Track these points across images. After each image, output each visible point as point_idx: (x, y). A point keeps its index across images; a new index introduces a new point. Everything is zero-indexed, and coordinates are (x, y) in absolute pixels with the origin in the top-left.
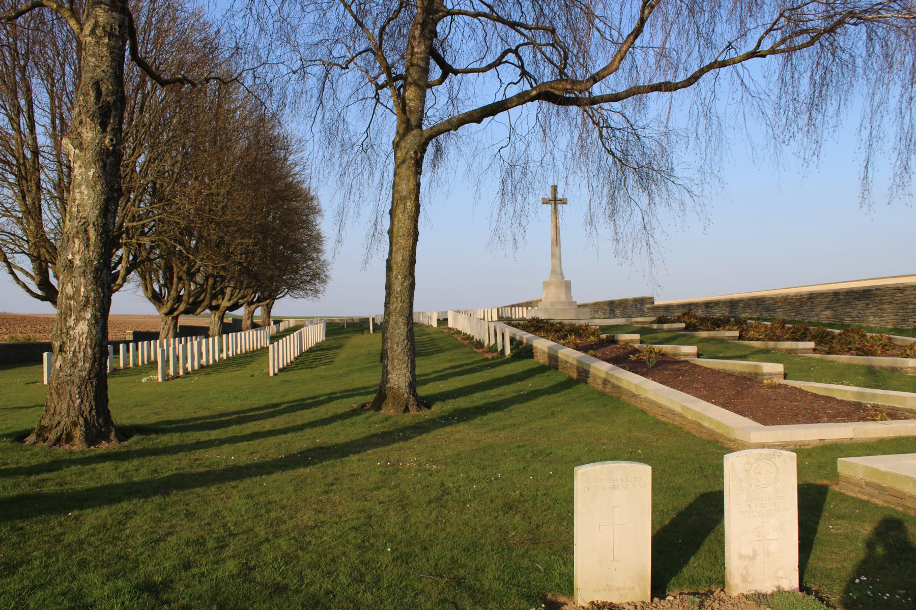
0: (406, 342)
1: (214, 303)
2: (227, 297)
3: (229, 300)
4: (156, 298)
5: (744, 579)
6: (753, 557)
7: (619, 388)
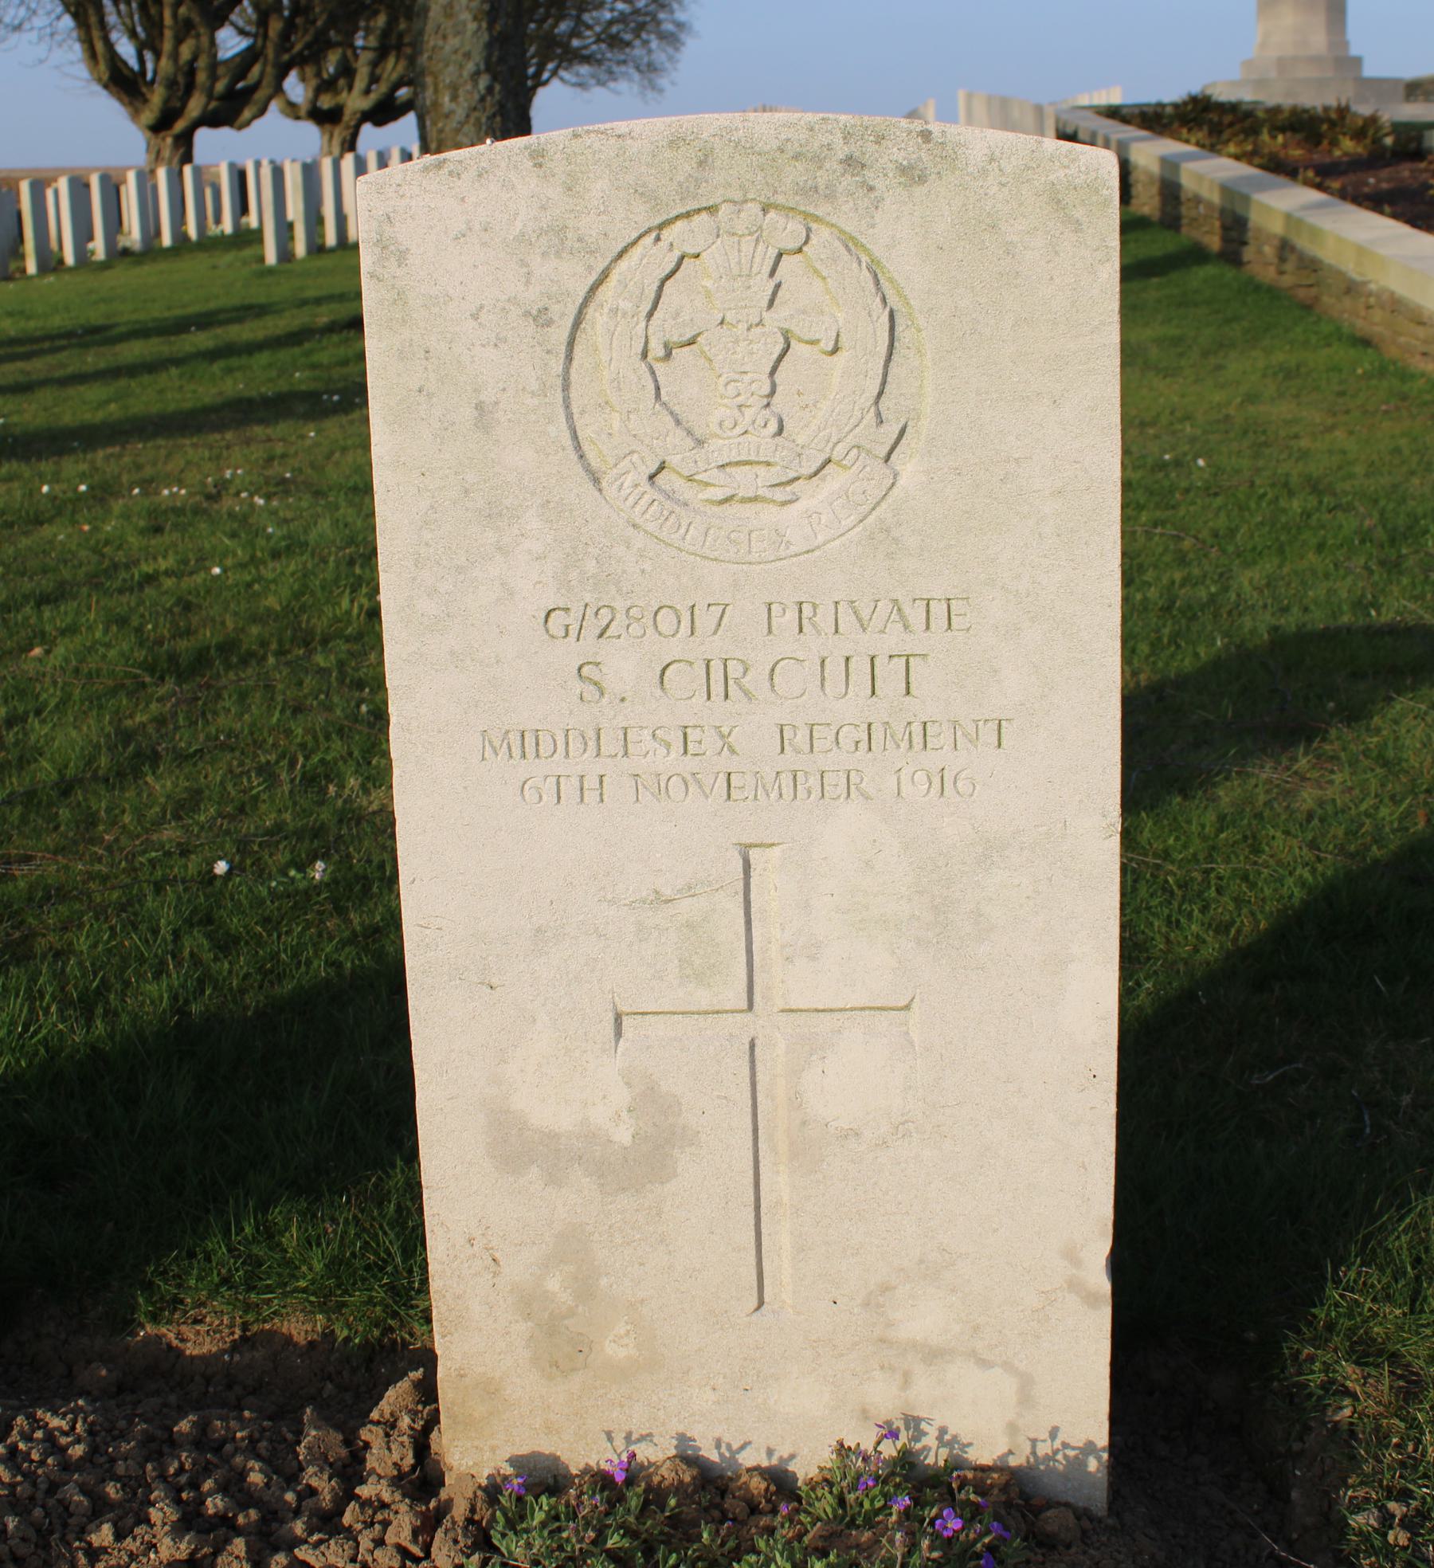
0: (484, 82)
1: (326, 102)
2: (360, 83)
3: (367, 92)
4: (124, 83)
5: (562, 1345)
6: (649, 1155)
7: (1311, 266)
